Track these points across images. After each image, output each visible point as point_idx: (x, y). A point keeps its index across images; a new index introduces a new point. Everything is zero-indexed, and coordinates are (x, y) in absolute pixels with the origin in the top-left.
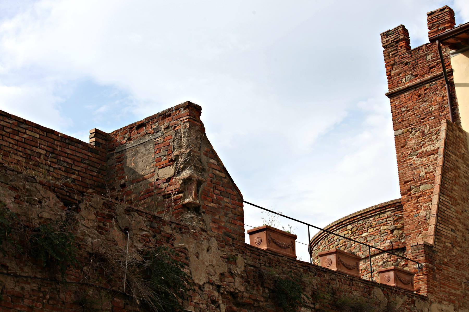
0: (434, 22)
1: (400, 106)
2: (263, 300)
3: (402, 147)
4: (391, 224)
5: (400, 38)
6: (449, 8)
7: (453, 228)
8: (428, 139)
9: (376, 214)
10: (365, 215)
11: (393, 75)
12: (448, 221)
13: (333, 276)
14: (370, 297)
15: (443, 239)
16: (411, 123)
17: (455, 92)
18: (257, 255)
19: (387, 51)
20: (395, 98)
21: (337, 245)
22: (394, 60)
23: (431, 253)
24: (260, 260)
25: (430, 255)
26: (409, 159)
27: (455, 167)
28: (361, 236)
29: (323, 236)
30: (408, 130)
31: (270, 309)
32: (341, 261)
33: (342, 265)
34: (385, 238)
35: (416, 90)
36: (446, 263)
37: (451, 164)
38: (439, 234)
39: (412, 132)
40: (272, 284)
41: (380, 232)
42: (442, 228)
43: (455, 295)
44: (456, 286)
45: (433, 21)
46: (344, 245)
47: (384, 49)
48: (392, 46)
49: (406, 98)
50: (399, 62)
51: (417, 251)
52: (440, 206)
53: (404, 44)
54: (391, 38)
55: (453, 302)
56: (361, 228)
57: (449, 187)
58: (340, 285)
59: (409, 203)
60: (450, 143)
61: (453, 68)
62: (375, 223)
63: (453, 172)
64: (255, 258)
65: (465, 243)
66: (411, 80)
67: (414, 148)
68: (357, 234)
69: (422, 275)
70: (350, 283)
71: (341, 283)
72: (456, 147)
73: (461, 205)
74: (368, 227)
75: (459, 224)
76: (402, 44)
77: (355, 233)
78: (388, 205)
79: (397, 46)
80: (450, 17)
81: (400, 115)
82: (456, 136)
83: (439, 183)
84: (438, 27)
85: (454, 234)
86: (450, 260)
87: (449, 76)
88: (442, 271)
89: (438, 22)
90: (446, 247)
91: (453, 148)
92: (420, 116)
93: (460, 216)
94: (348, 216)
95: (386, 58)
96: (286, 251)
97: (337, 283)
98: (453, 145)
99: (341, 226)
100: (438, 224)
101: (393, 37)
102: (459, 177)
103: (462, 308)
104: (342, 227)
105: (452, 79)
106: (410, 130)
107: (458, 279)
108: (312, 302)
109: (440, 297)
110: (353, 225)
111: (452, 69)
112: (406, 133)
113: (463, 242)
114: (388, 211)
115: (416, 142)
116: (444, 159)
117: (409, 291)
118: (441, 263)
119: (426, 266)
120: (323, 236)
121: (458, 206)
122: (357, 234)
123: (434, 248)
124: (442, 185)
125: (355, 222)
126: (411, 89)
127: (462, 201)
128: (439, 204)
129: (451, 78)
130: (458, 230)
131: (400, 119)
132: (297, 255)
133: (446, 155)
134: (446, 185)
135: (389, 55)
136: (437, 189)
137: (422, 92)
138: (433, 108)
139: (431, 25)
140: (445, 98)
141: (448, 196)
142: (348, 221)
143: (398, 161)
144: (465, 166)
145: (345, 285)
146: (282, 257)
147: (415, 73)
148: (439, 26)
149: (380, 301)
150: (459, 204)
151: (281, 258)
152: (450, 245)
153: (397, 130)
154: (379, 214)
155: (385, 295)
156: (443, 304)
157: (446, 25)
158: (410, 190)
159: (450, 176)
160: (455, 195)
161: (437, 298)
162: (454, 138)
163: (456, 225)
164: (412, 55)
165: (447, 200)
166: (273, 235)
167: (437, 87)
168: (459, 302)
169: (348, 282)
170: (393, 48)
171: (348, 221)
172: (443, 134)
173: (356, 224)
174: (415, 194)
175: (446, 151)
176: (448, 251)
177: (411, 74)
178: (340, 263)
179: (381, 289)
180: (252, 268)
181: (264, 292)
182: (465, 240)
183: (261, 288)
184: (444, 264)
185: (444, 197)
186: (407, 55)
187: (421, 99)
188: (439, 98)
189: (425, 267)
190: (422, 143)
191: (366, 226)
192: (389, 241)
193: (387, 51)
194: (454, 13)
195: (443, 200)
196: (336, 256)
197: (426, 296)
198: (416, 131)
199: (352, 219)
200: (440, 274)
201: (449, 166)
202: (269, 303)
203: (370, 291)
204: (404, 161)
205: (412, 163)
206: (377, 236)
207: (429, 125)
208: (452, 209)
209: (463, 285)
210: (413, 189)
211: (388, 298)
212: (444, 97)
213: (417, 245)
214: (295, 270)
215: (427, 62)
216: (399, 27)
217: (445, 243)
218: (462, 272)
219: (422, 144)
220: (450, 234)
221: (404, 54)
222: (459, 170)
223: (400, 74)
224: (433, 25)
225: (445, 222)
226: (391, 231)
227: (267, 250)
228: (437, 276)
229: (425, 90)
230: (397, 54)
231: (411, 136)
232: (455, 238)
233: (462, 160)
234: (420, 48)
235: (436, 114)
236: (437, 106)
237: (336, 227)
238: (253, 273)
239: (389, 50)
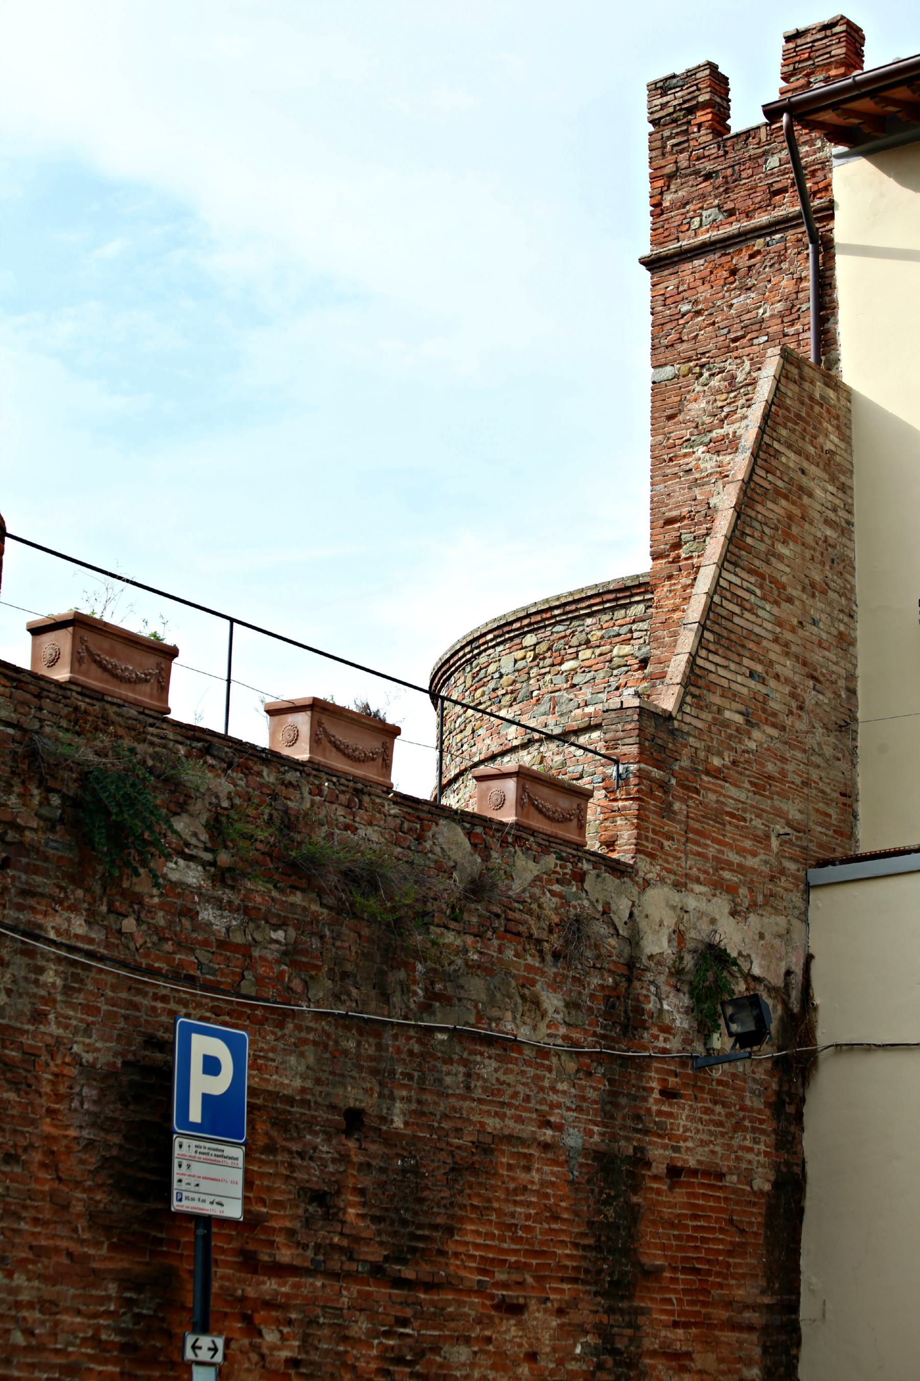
0: (799, 62)
1: (678, 298)
2: (35, 826)
3: (670, 418)
4: (642, 641)
5: (701, 99)
6: (849, 23)
7: (759, 668)
8: (742, 401)
9: (604, 609)
10: (573, 607)
11: (668, 204)
12: (743, 646)
13: (292, 776)
14: (420, 848)
15: (716, 699)
16: (700, 350)
17: (832, 268)
18: (35, 696)
19: (658, 136)
20: (666, 272)
21: (494, 690)
22: (676, 162)
23: (664, 735)
24: (40, 709)
25: (660, 742)
26: (685, 455)
27: (794, 489)
28: (557, 668)
29: (460, 659)
30: (690, 370)
31: (60, 854)
32: (325, 732)
33: (329, 745)
34: (622, 681)
35: (725, 255)
36: (719, 770)
37: (781, 479)
38: (701, 682)
39: (701, 375)
40: (75, 781)
41: (610, 661)
42: (717, 664)
43: (741, 869)
44: (748, 844)
45: (797, 59)
46: (512, 692)
47: (651, 128)
48: (674, 121)
49: (697, 275)
50: (689, 171)
51: (620, 727)
52: (717, 599)
53: (709, 117)
54: (674, 99)
55: (731, 890)
56: (559, 645)
57: (762, 547)
58: (313, 803)
59: (671, 585)
60: (784, 417)
61: (836, 199)
62: (599, 633)
63: (783, 502)
64: (23, 703)
65: (800, 716)
66: (717, 226)
67: (703, 424)
68: (548, 661)
69: (626, 799)
70: (350, 801)
71: (318, 798)
72: (805, 430)
73: (797, 602)
74: (580, 645)
75: (782, 659)
76: (703, 116)
77: (544, 658)
78: (639, 585)
79: (689, 123)
80: (848, 49)
81: (675, 323)
82: (811, 398)
83: (724, 532)
84: (808, 75)
85: (760, 687)
86: (734, 763)
87: (820, 220)
88: (698, 793)
89: (811, 62)
90: (726, 724)
91: (793, 431)
92: (729, 332)
93: (788, 636)
94: (527, 608)
95: (654, 154)
96: (134, 691)
97: (302, 798)
98: (797, 424)
99: (507, 636)
100: (703, 653)
101: (679, 94)
102: (803, 518)
103: (760, 912)
104: (511, 639)
105: (831, 230)
106: (697, 370)
107: (757, 823)
108: (209, 845)
109: (680, 871)
110: (541, 634)
111: (832, 202)
112: (684, 376)
113: (791, 713)
114: (638, 602)
115: (710, 407)
116: (755, 463)
117: (564, 841)
118: (696, 770)
119: (641, 775)
120: (460, 659)
121: (785, 605)
122: (548, 661)
123: (676, 723)
124: (734, 539)
125: (545, 627)
126: (713, 251)
127: (804, 590)
128: (715, 592)
129: (828, 228)
130: (777, 677)
131: (674, 336)
132: (171, 704)
133: (761, 451)
134: (749, 540)
135: (664, 147)
136: (715, 547)
137: (742, 260)
138: (766, 311)
139: (791, 67)
140: (804, 284)
141: (751, 572)
142: (526, 622)
143: (653, 457)
144: (831, 488)
145: (334, 806)
146: (119, 706)
147: (730, 205)
148: (812, 73)
149: (455, 862)
150: (790, 600)
151: (115, 709)
152: (739, 719)
153: (660, 366)
154: (612, 609)
155: (474, 846)
156: (692, 891)
157: (833, 72)
158: (677, 545)
159: (771, 515)
160: (782, 571)
161: (669, 871)
162: (802, 403)
163: (771, 662)
164: (726, 152)
165: (745, 584)
166: (93, 641)
167: (786, 249)
168: (751, 890)
169: (343, 798)
170: (678, 126)
171: (526, 622)
172: (764, 390)
173: (548, 633)
174: (691, 558)
175: (767, 439)
176: (730, 737)
177: (719, 207)
178: (324, 741)
179: (464, 828)
180: (10, 731)
181: (45, 802)
182: (801, 708)
183: (36, 792)
184: (708, 773)
185: (736, 575)
186: (713, 150)
187: (737, 283)
188: (786, 284)
189: (635, 776)
190: (726, 410)
191: (574, 642)
192: (631, 691)
193: (658, 136)
194: (863, 38)
195: (730, 582)
196: (312, 718)
197: (631, 862)
198: (713, 375)
199: (538, 618)
200: (690, 803)
201: (770, 482)
202: (56, 837)
203: (422, 830)
204: (671, 460)
205: (690, 466)
206: (601, 674)
207: (752, 359)
208: (761, 613)
209: (775, 843)
210: (686, 543)
211: (486, 858)
212: (801, 279)
213: (621, 708)
214: (157, 749)
215: (767, 176)
216: (699, 67)
217: (720, 710)
218: (777, 803)
219: (724, 414)
220: (744, 686)
221: (704, 148)
222: (806, 500)
223: (687, 203)
224: (795, 69)
225: (728, 648)
226: (641, 661)
227: (71, 681)
228: (677, 806)
229: (751, 256)
230: (686, 145)
231: (698, 388)
232: (761, 699)
233: (824, 470)
234: (752, 133)
235: (774, 328)
236: (779, 307)
237: (495, 637)
238: (12, 746)
239: (667, 133)
